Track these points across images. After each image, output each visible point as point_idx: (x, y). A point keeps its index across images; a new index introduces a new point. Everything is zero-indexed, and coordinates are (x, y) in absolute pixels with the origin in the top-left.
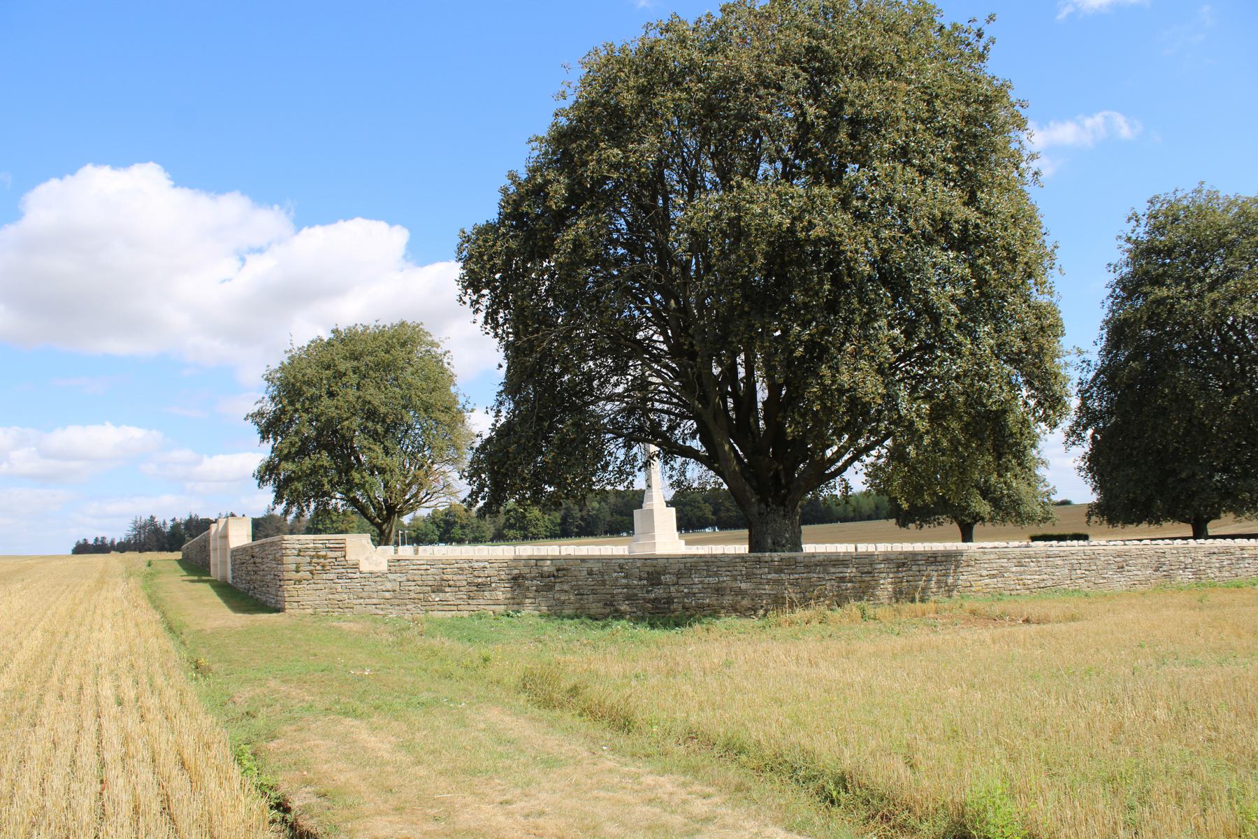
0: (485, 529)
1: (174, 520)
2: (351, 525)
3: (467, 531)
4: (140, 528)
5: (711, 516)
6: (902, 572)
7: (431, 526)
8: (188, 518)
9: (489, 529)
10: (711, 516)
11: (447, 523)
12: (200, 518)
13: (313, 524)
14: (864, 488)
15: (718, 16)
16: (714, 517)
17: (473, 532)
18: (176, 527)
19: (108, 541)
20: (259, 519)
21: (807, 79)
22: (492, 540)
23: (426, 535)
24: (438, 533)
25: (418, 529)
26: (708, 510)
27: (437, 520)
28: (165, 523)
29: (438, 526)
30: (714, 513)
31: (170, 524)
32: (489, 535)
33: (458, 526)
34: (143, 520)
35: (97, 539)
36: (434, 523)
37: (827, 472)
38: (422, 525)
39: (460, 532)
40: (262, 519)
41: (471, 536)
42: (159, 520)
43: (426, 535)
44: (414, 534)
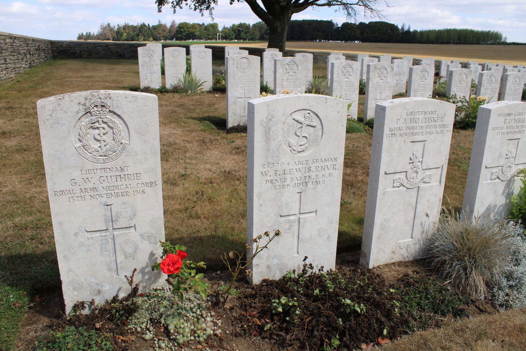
0: (256, 34)
1: (118, 25)
2: (196, 30)
3: (248, 35)
4: (104, 29)
5: (359, 36)
6: (411, 293)
7: (232, 32)
8: (124, 24)
9: (257, 34)
10: (359, 36)
11: (239, 30)
12: (130, 25)
13: (179, 29)
14: (186, 248)
15: (464, 167)
16: (361, 36)
17: (250, 35)
18: (119, 28)
19: (92, 34)
20: (155, 26)
21: (373, 346)
22: (258, 40)
23: (230, 36)
24: (234, 35)
25: (226, 33)
26: (358, 32)
27: (234, 29)
28: (114, 27)
29: (235, 32)
30: (361, 34)
31: (116, 27)
32: (258, 37)
33: (244, 32)
34: (105, 25)
35: (87, 33)
36: (233, 30)
37: (296, 17)
38: (227, 31)
39: (245, 35)
40: (157, 26)
41: (249, 37)
42: (112, 25)
43: (230, 36)
44: (224, 35)
